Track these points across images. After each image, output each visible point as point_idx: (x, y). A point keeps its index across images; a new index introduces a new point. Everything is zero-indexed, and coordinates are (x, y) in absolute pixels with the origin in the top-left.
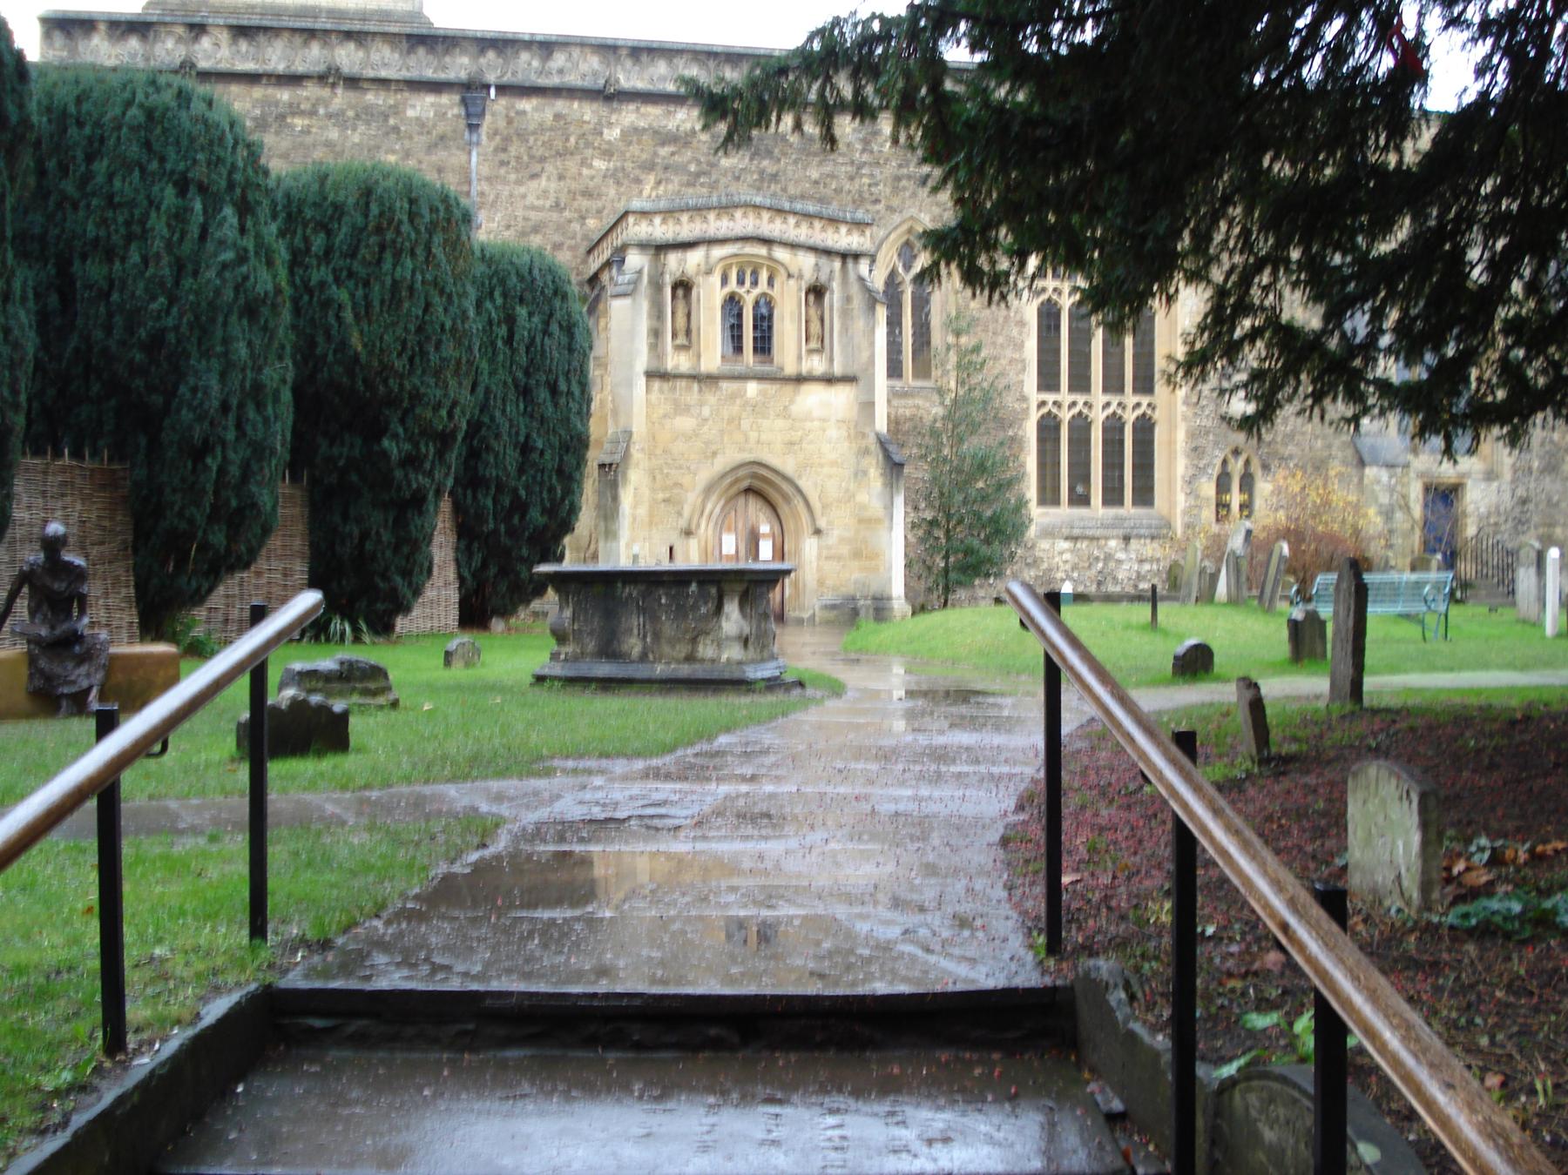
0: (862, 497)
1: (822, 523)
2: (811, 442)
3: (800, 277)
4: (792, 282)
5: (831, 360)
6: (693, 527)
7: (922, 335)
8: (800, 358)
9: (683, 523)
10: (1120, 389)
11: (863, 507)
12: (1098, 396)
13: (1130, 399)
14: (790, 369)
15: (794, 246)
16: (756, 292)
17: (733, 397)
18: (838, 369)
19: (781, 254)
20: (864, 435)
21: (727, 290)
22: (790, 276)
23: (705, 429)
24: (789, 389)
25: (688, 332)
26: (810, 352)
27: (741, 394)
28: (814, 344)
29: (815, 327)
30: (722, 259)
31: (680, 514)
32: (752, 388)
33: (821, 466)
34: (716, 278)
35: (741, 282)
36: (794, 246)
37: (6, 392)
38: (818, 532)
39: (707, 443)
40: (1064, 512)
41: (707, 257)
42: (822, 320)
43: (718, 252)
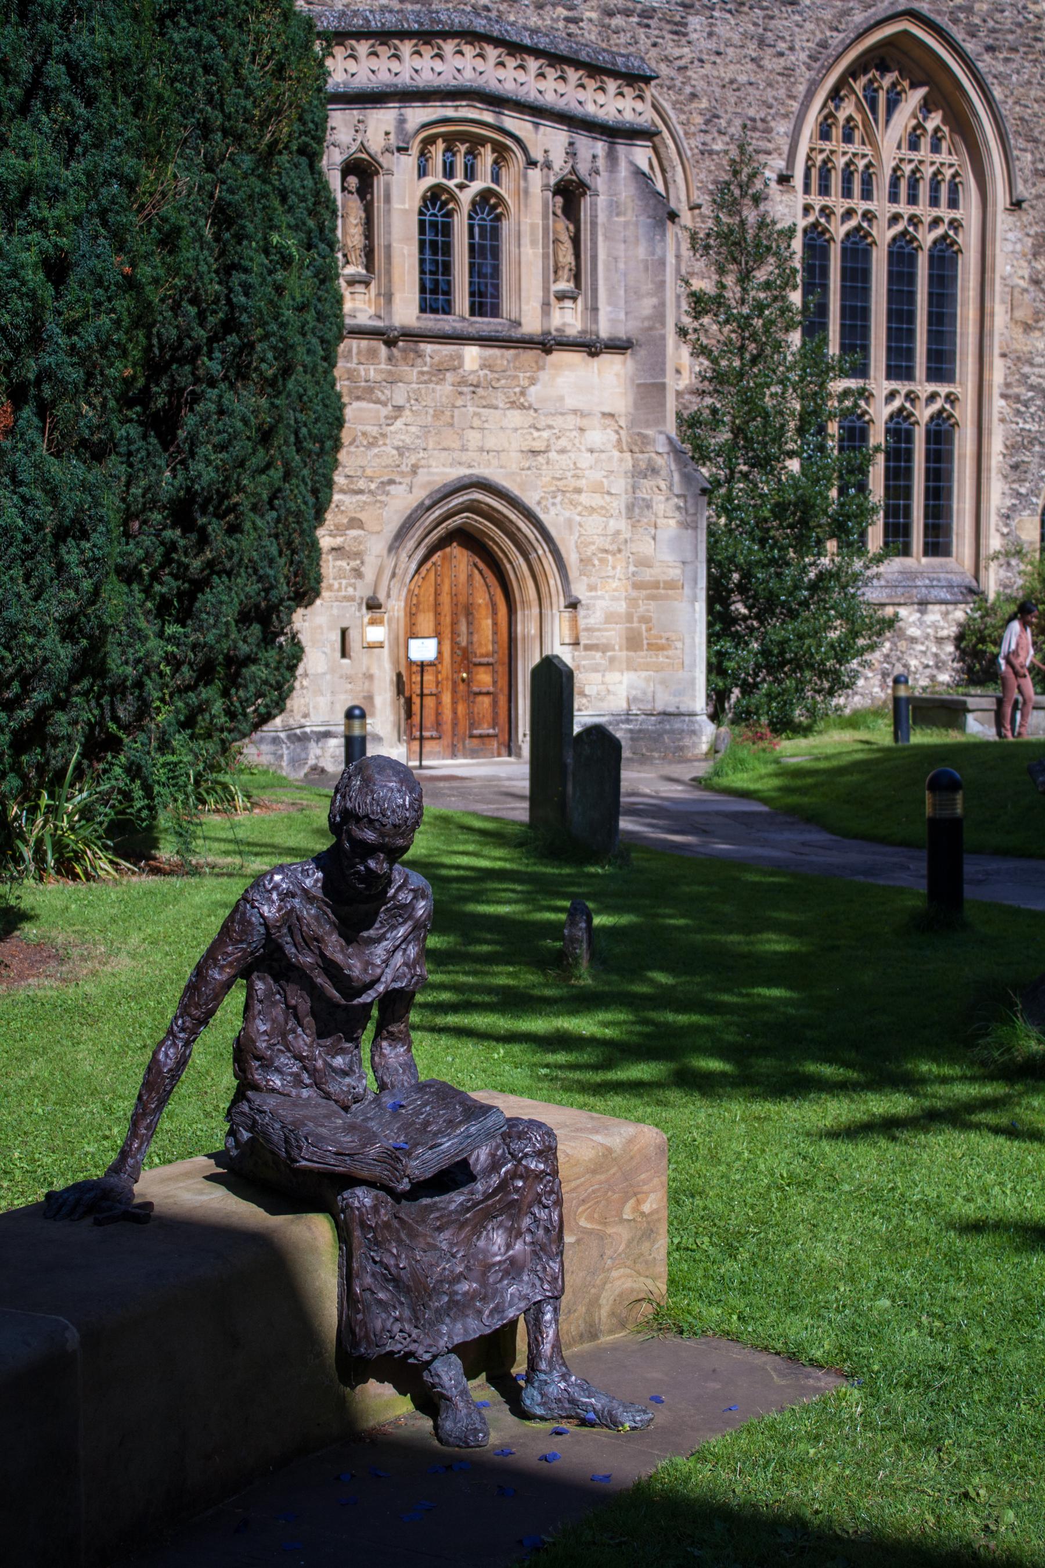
0: (645, 547)
1: (579, 590)
2: (562, 451)
3: (548, 165)
4: (535, 175)
5: (388, 297)
6: (382, 597)
7: (941, 296)
8: (546, 305)
9: (363, 590)
10: (907, 374)
11: (644, 562)
12: (880, 384)
13: (924, 388)
14: (532, 325)
15: (537, 112)
16: (477, 186)
17: (440, 371)
18: (604, 331)
19: (512, 122)
20: (645, 441)
21: (429, 181)
22: (532, 163)
23: (399, 424)
24: (530, 356)
25: (369, 253)
26: (561, 297)
27: (454, 365)
28: (564, 285)
29: (567, 257)
30: (425, 126)
31: (358, 573)
32: (472, 354)
33: (578, 491)
34: (409, 162)
35: (449, 172)
36: (537, 112)
37: (765, 4)
38: (573, 605)
39: (401, 450)
40: (918, 561)
41: (402, 121)
42: (576, 241)
43: (418, 115)
